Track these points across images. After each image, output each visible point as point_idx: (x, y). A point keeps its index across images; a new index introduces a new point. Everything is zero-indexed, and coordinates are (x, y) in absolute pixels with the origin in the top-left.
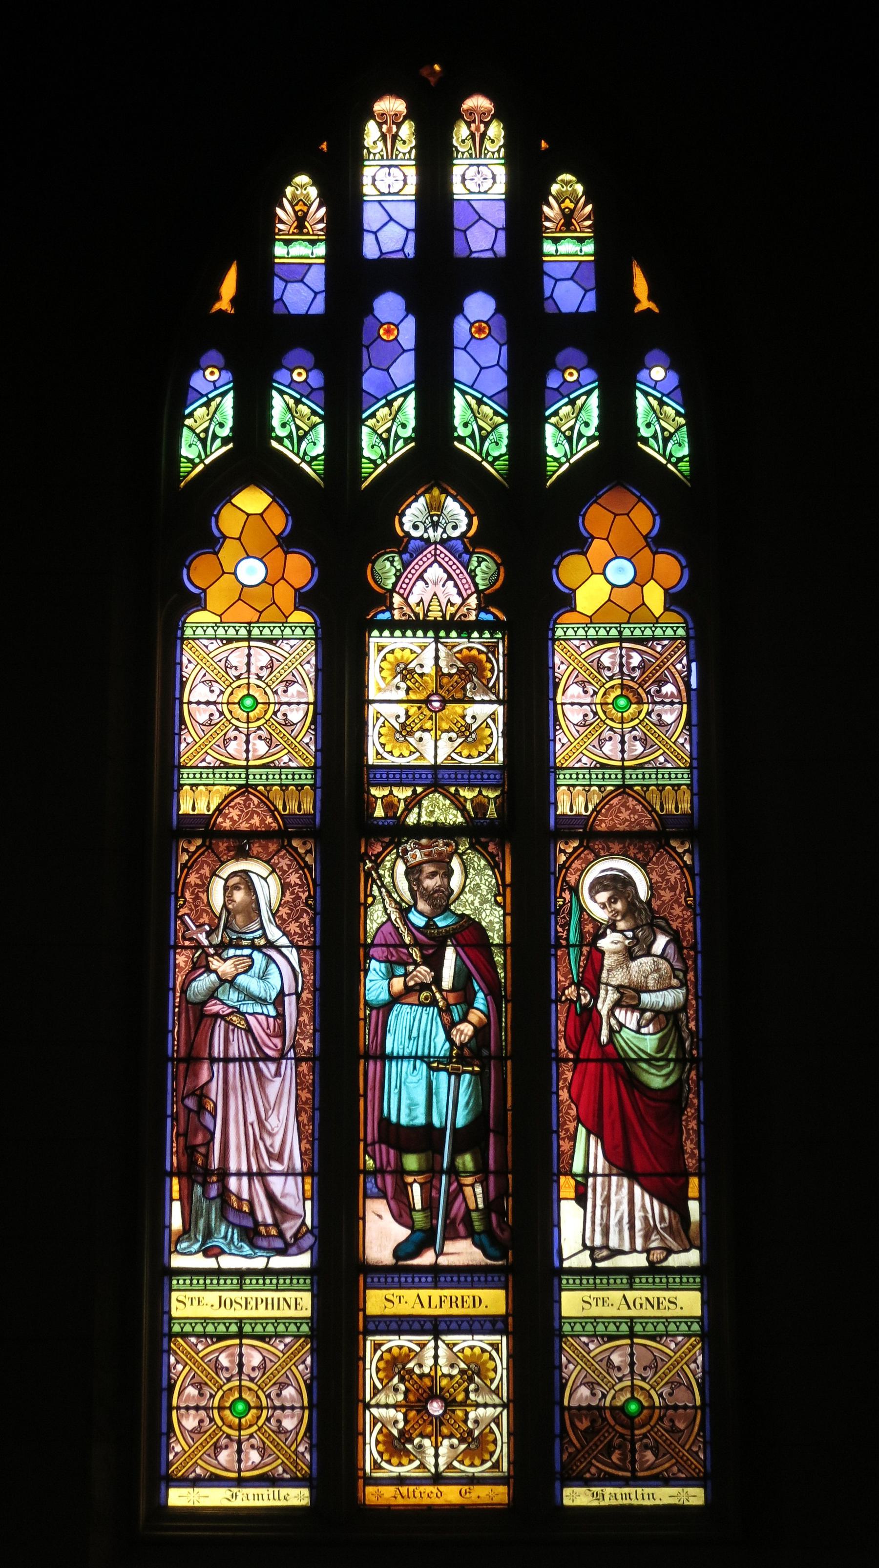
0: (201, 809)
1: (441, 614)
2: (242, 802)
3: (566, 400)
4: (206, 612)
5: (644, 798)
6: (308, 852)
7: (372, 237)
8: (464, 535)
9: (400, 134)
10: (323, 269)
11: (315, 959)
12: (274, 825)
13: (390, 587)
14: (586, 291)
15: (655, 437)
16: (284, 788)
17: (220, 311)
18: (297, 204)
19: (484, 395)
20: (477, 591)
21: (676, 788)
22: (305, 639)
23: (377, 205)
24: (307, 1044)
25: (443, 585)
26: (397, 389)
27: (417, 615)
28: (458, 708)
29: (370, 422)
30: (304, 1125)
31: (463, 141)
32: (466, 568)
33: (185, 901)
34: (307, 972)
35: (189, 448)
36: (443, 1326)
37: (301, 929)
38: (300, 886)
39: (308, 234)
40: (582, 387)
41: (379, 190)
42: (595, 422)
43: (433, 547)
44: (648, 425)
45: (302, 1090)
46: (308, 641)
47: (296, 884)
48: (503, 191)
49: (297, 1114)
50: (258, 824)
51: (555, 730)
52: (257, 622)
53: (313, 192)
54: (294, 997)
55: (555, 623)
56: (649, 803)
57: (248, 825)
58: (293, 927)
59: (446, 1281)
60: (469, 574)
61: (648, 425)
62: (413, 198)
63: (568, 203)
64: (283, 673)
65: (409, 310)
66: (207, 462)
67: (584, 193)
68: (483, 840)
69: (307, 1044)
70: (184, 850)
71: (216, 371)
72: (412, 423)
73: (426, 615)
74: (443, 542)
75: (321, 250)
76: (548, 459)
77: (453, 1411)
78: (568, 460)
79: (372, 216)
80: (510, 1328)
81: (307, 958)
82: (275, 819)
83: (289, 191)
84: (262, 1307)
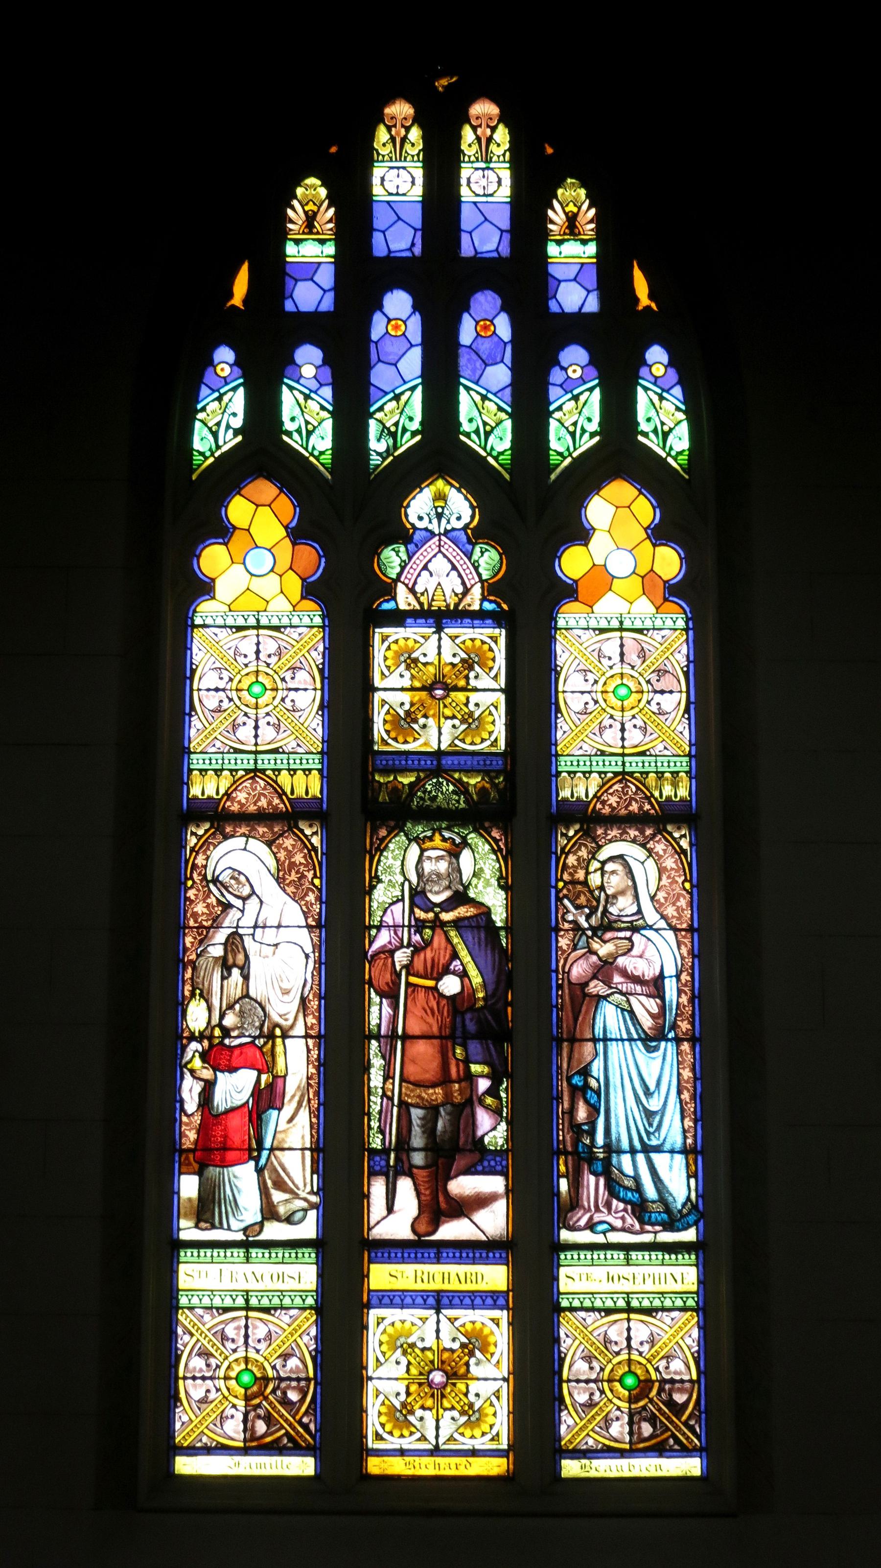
0: (211, 791)
1: (444, 604)
2: (620, 789)
3: (569, 396)
4: (577, 603)
5: (276, 782)
6: (315, 833)
7: (382, 235)
8: (466, 526)
9: (409, 136)
10: (332, 268)
11: (692, 942)
12: (282, 806)
13: (394, 576)
14: (589, 292)
15: (655, 431)
16: (292, 773)
17: (233, 306)
18: (307, 204)
19: (488, 391)
20: (482, 581)
21: (307, 773)
22: (675, 630)
23: (386, 205)
24: (684, 1026)
25: (448, 575)
26: (405, 382)
27: (448, 606)
28: (460, 696)
29: (378, 415)
30: (686, 1103)
31: (384, 145)
32: (470, 559)
33: (194, 882)
34: (685, 955)
35: (201, 440)
36: (445, 1301)
37: (678, 913)
38: (677, 871)
39: (318, 233)
40: (585, 383)
41: (387, 191)
42: (418, 417)
43: (437, 538)
44: (293, 419)
45: (684, 1068)
46: (679, 631)
47: (301, 864)
48: (421, 194)
49: (679, 1092)
50: (265, 806)
51: (557, 718)
52: (265, 611)
53: (323, 192)
54: (674, 979)
55: (557, 613)
56: (281, 787)
57: (255, 808)
58: (670, 911)
59: (448, 1257)
60: (473, 565)
61: (649, 420)
62: (420, 199)
63: (310, 207)
64: (289, 659)
65: (416, 308)
66: (575, 455)
67: (328, 197)
68: (487, 824)
69: (684, 1026)
70: (193, 834)
71: (218, 368)
72: (596, 419)
73: (430, 605)
74: (446, 533)
75: (330, 249)
76: (195, 453)
77: (454, 1385)
78: (212, 454)
79: (381, 218)
80: (511, 1305)
81: (686, 941)
82: (651, 803)
83: (300, 191)
84: (649, 1281)
